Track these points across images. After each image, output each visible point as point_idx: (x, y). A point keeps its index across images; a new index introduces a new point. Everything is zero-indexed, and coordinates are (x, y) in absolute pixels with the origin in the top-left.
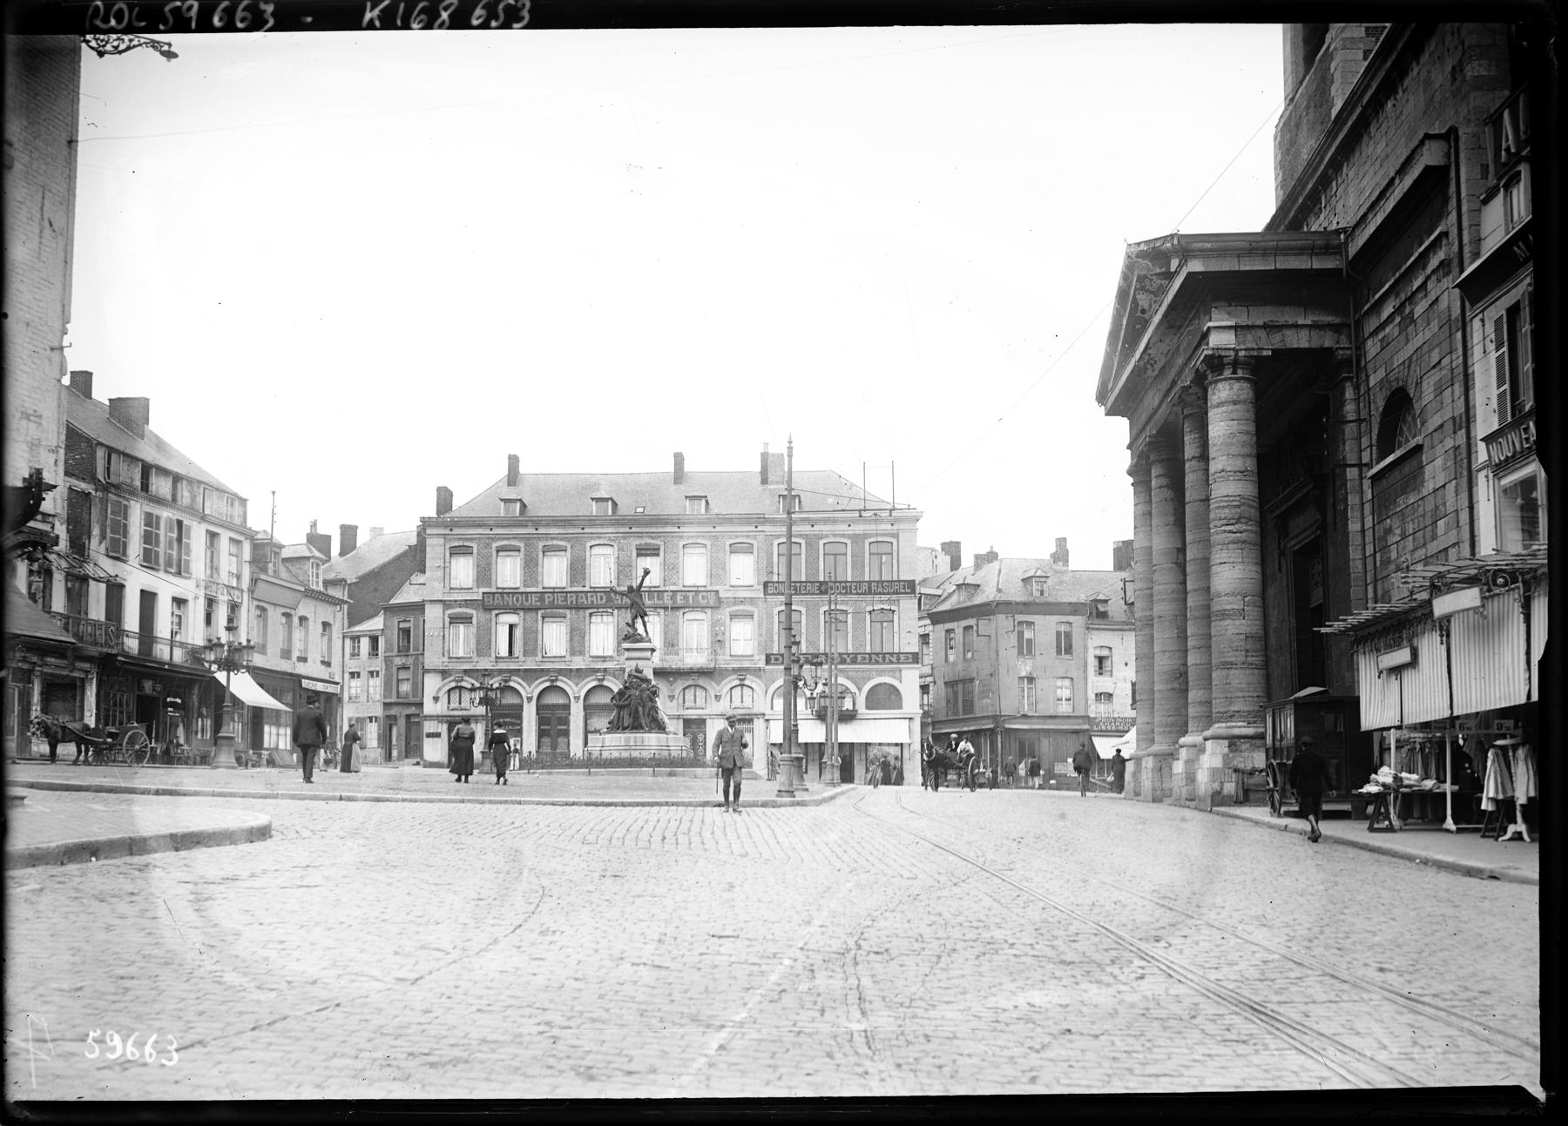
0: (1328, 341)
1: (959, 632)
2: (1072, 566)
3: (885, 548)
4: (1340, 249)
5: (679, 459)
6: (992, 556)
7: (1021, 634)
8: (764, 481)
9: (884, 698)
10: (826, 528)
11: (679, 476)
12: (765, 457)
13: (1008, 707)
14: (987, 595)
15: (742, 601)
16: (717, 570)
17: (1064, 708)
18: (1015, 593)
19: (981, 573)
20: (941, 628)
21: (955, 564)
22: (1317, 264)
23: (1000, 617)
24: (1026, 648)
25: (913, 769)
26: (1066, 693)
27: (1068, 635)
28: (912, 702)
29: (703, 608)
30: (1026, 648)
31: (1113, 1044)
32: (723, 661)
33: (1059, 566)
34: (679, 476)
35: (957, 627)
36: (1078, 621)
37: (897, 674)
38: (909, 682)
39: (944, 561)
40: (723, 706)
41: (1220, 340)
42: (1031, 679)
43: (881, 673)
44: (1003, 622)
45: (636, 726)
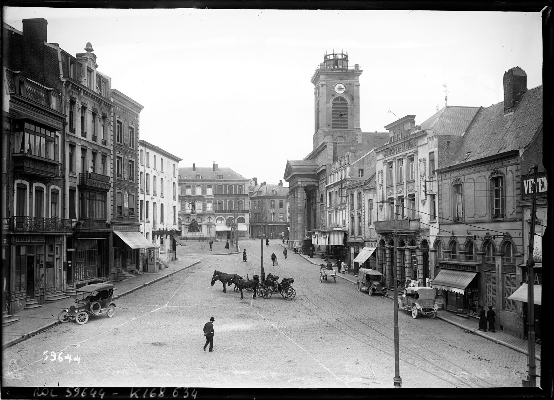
0: (314, 183)
1: (257, 202)
2: (283, 186)
3: (241, 188)
4: (316, 171)
5: (194, 164)
6: (265, 183)
7: (271, 204)
8: (214, 170)
9: (242, 220)
10: (229, 182)
11: (194, 168)
12: (214, 164)
13: (268, 220)
14: (264, 194)
15: (210, 199)
16: (204, 191)
17: (281, 220)
18: (270, 194)
19: (262, 188)
20: (253, 201)
21: (256, 184)
22: (313, 173)
23: (267, 200)
24: (273, 206)
25: (249, 236)
26: (281, 217)
27: (282, 204)
28: (247, 222)
29: (201, 200)
30: (273, 206)
31: (43, 275)
32: (206, 212)
33: (280, 187)
34: (194, 168)
35: (257, 201)
36: (284, 200)
37: (244, 215)
38: (247, 217)
39: (253, 183)
40: (205, 222)
41: (299, 183)
42: (274, 214)
43: (240, 215)
44: (267, 200)
45: (194, 231)
